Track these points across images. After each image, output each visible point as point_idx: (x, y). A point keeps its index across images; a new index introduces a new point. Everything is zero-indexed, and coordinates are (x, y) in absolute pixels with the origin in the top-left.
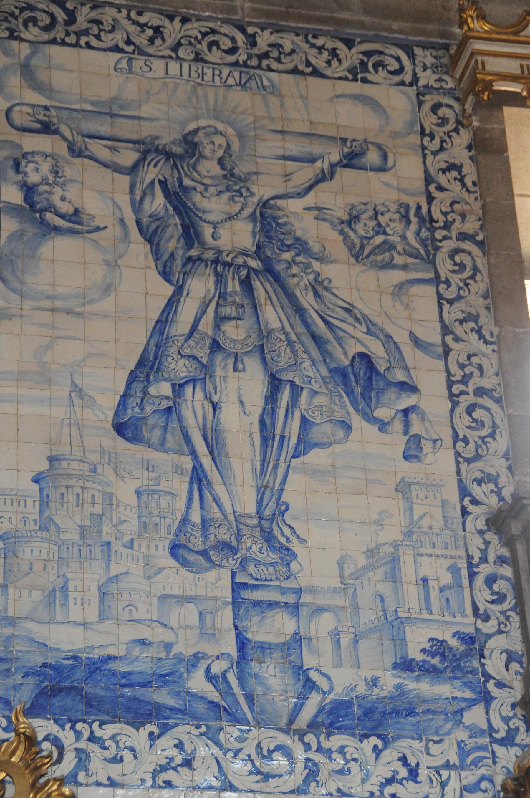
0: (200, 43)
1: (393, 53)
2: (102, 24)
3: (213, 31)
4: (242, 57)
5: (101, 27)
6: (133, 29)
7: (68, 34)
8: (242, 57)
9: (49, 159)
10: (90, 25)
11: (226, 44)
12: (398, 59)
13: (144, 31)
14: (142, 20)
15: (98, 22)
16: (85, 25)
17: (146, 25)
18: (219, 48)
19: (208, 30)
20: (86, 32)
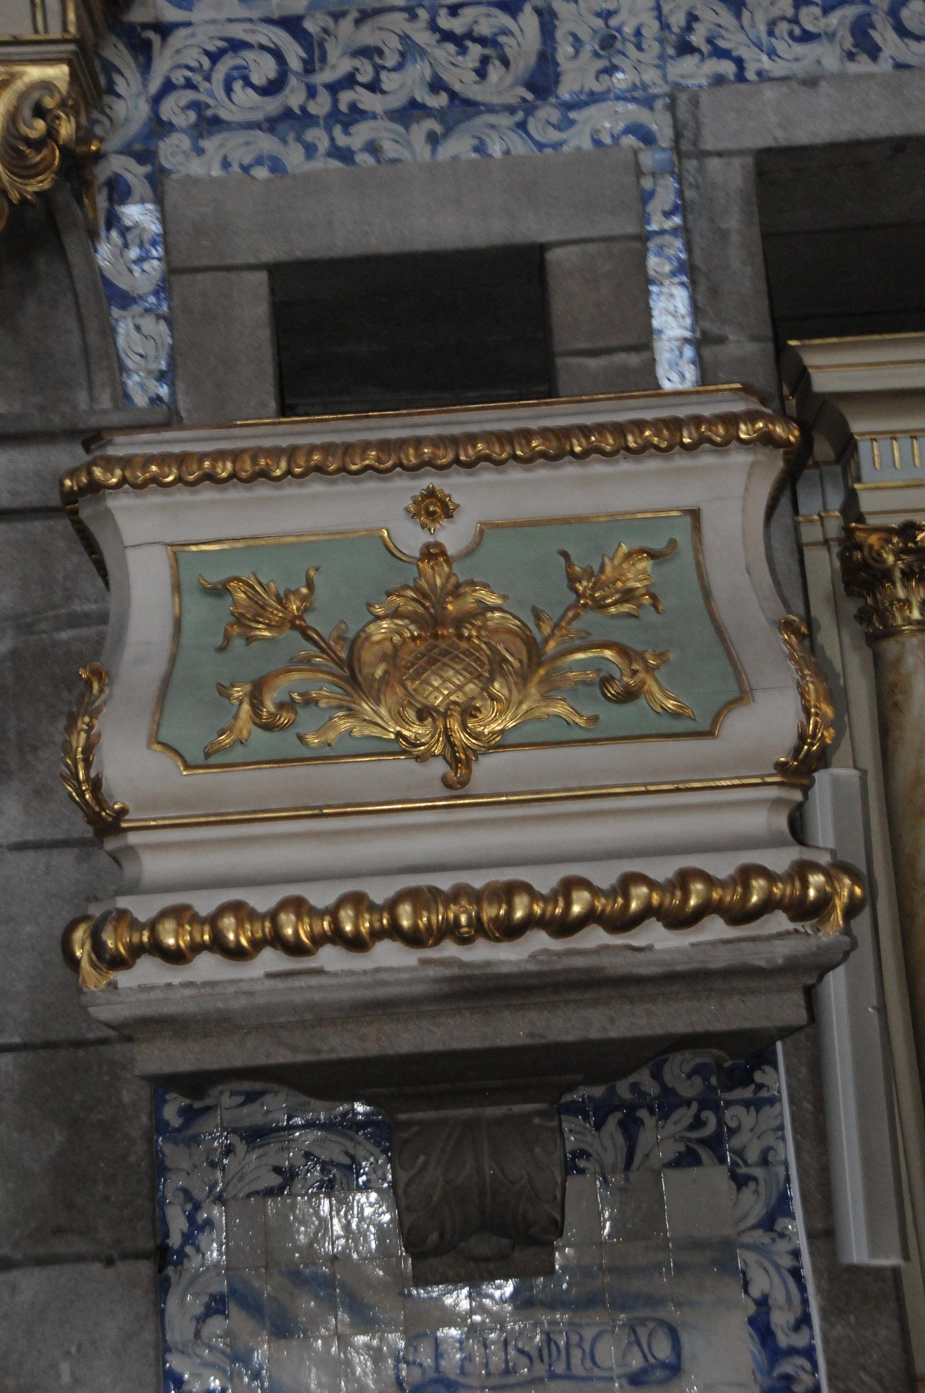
0: (208, 78)
1: (265, 41)
2: (380, 53)
3: (236, 46)
4: (294, 97)
5: (378, 61)
6: (730, 41)
7: (312, 92)
8: (294, 97)
9: (846, 939)
10: (357, 63)
11: (263, 69)
12: (277, 54)
13: (463, 51)
14: (456, 25)
15: (366, 52)
16: (345, 66)
17: (470, 35)
18: (248, 83)
19: (221, 44)
20: (349, 81)
